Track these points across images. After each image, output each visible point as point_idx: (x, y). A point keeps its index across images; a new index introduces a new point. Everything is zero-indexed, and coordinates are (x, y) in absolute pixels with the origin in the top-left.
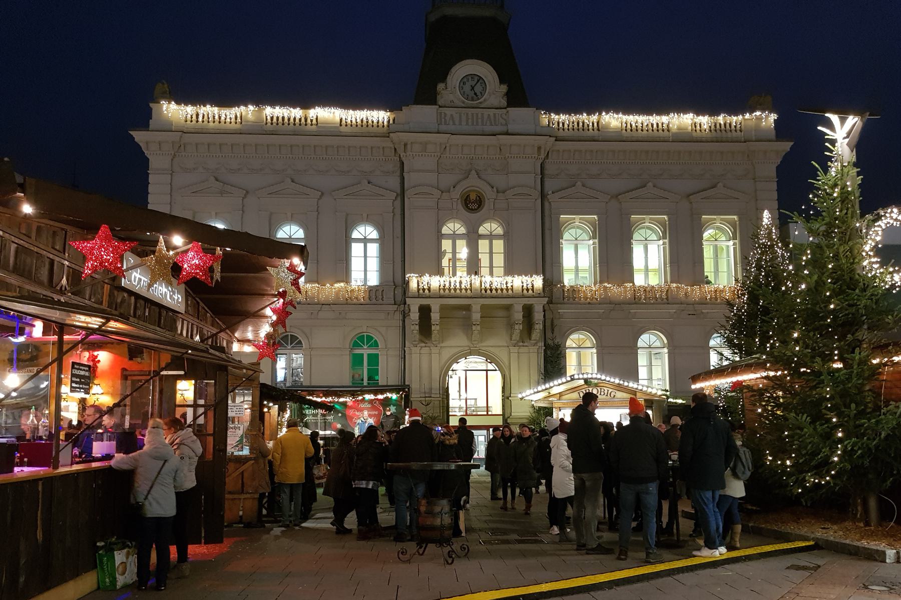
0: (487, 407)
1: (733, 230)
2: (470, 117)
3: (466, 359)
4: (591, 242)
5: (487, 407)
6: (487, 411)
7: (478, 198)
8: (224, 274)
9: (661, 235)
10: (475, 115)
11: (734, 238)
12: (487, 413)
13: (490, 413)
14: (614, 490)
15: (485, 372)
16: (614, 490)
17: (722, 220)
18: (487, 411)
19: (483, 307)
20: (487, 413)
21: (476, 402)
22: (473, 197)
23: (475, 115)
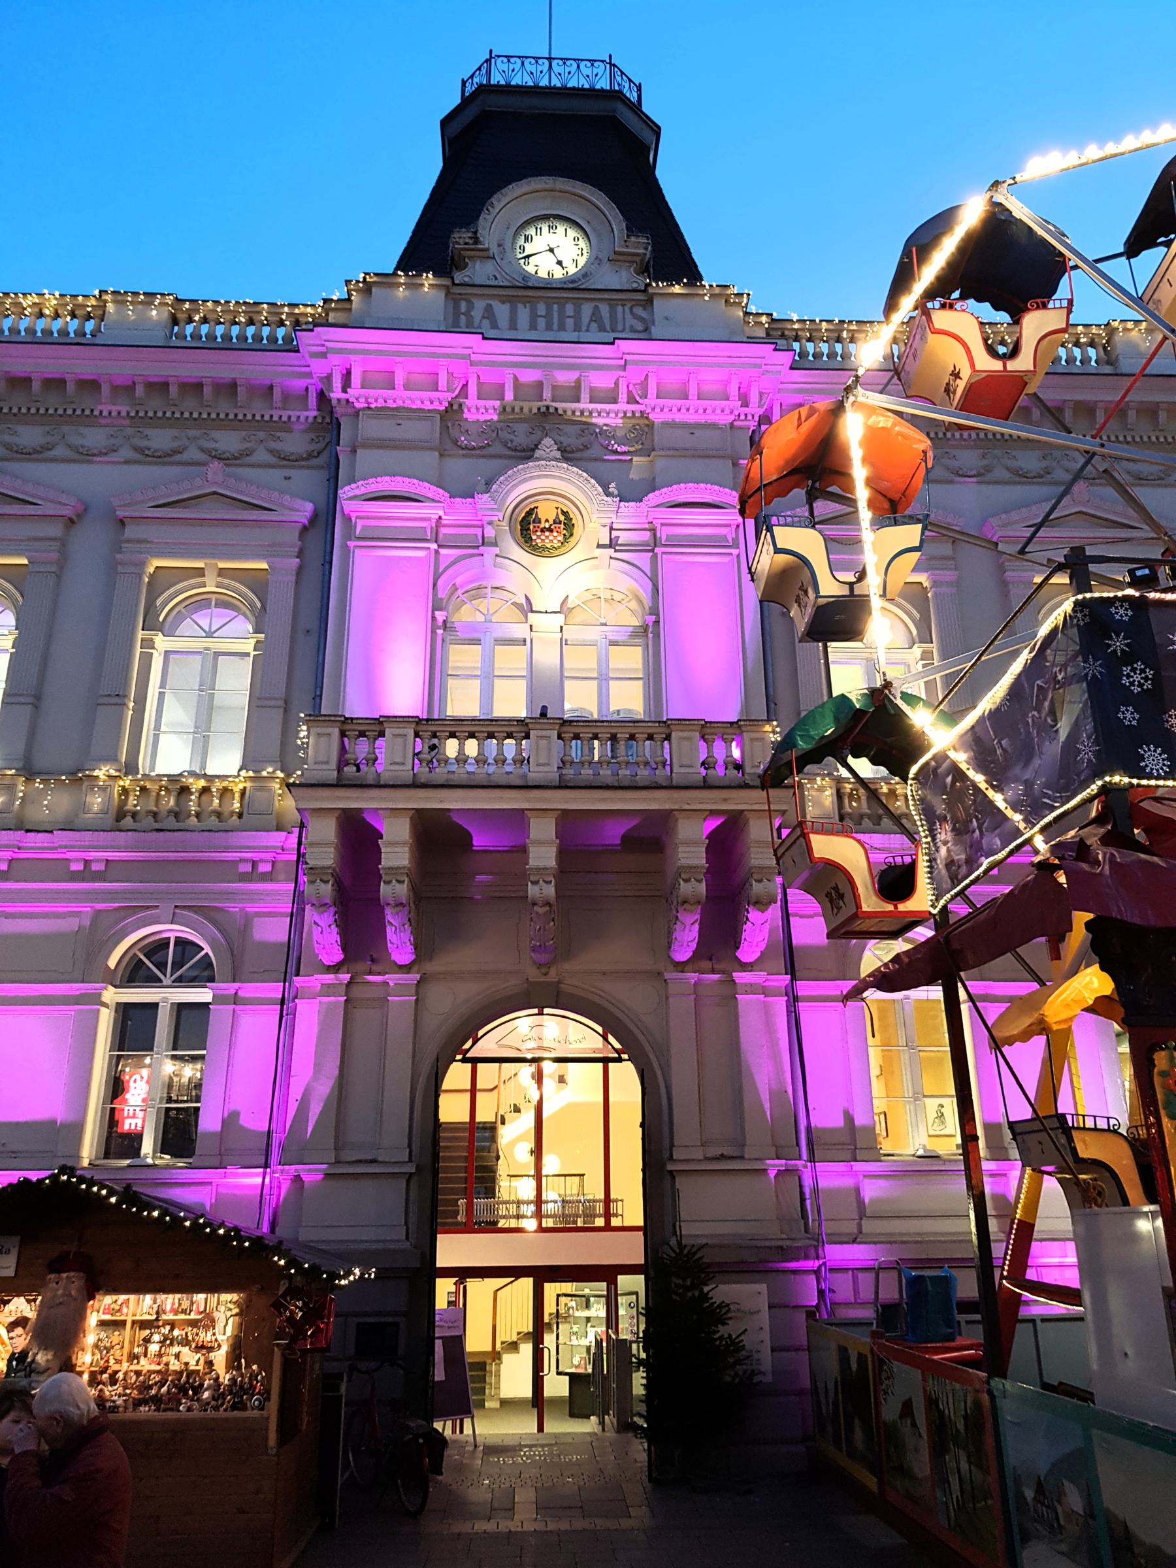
0: (607, 1200)
1: (918, 616)
2: (570, 322)
3: (541, 1013)
4: (917, 651)
5: (607, 1200)
6: (608, 1215)
7: (562, 518)
8: (480, 1397)
9: (914, 632)
10: (555, 326)
11: (925, 637)
12: (608, 1221)
13: (615, 1222)
14: (674, 1297)
15: (600, 1065)
16: (674, 1297)
17: (222, 572)
18: (608, 1215)
19: (567, 821)
20: (608, 1221)
21: (581, 1185)
22: (547, 512)
23: (555, 326)
